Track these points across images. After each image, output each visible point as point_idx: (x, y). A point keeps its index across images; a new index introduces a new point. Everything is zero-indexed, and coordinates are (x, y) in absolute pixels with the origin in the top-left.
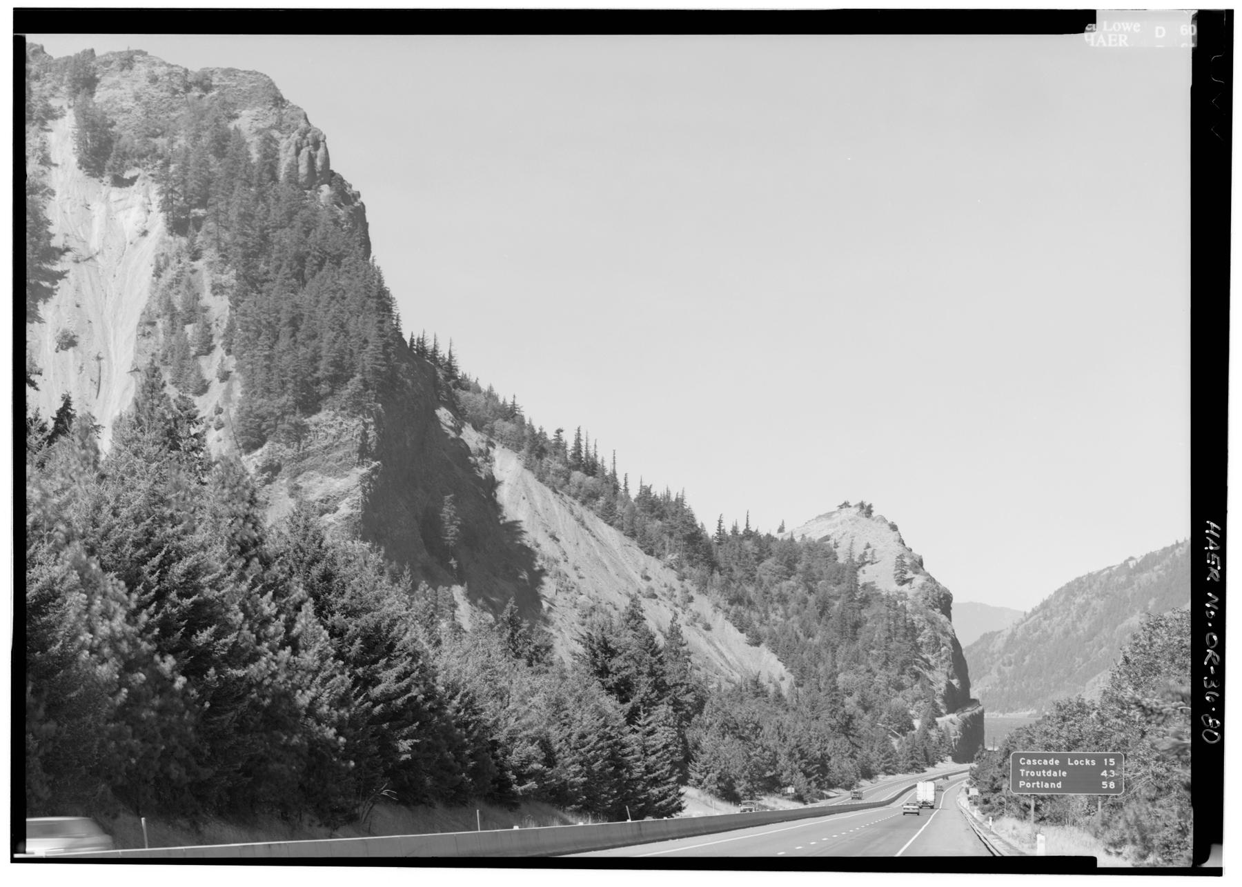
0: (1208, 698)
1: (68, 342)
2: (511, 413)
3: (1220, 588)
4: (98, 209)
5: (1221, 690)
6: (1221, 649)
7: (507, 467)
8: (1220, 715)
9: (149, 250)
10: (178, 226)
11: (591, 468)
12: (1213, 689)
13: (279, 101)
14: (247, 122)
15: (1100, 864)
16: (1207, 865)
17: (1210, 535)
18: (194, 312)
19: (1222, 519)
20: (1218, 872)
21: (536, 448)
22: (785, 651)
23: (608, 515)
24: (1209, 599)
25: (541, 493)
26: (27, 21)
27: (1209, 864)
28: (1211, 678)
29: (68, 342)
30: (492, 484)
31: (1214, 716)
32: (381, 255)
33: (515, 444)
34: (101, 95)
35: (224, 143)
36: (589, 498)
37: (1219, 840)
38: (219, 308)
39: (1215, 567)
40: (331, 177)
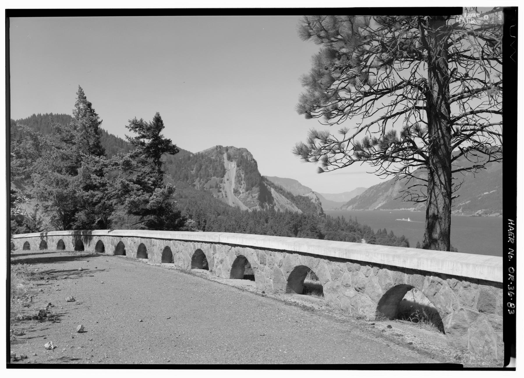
0: (509, 294)
1: (228, 180)
2: (273, 184)
3: (514, 246)
4: (229, 165)
5: (515, 291)
6: (515, 274)
7: (273, 190)
8: (514, 301)
9: (235, 168)
10: (238, 166)
11: (281, 190)
12: (511, 290)
13: (248, 151)
14: (244, 154)
15: (464, 367)
16: (508, 366)
17: (510, 225)
18: (240, 176)
19: (514, 218)
20: (514, 369)
21: (276, 188)
22: (302, 210)
23: (283, 195)
24: (510, 251)
25: (276, 193)
26: (10, 13)
27: (509, 366)
28: (511, 286)
29: (228, 180)
30: (270, 192)
31: (512, 302)
32: (259, 168)
33: (273, 188)
34: (229, 151)
35: (242, 157)
36: (281, 193)
37: (514, 356)
38: (243, 176)
39: (512, 237)
40: (254, 160)
